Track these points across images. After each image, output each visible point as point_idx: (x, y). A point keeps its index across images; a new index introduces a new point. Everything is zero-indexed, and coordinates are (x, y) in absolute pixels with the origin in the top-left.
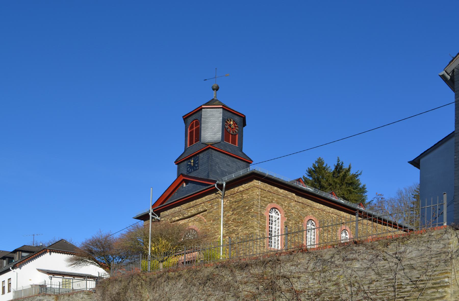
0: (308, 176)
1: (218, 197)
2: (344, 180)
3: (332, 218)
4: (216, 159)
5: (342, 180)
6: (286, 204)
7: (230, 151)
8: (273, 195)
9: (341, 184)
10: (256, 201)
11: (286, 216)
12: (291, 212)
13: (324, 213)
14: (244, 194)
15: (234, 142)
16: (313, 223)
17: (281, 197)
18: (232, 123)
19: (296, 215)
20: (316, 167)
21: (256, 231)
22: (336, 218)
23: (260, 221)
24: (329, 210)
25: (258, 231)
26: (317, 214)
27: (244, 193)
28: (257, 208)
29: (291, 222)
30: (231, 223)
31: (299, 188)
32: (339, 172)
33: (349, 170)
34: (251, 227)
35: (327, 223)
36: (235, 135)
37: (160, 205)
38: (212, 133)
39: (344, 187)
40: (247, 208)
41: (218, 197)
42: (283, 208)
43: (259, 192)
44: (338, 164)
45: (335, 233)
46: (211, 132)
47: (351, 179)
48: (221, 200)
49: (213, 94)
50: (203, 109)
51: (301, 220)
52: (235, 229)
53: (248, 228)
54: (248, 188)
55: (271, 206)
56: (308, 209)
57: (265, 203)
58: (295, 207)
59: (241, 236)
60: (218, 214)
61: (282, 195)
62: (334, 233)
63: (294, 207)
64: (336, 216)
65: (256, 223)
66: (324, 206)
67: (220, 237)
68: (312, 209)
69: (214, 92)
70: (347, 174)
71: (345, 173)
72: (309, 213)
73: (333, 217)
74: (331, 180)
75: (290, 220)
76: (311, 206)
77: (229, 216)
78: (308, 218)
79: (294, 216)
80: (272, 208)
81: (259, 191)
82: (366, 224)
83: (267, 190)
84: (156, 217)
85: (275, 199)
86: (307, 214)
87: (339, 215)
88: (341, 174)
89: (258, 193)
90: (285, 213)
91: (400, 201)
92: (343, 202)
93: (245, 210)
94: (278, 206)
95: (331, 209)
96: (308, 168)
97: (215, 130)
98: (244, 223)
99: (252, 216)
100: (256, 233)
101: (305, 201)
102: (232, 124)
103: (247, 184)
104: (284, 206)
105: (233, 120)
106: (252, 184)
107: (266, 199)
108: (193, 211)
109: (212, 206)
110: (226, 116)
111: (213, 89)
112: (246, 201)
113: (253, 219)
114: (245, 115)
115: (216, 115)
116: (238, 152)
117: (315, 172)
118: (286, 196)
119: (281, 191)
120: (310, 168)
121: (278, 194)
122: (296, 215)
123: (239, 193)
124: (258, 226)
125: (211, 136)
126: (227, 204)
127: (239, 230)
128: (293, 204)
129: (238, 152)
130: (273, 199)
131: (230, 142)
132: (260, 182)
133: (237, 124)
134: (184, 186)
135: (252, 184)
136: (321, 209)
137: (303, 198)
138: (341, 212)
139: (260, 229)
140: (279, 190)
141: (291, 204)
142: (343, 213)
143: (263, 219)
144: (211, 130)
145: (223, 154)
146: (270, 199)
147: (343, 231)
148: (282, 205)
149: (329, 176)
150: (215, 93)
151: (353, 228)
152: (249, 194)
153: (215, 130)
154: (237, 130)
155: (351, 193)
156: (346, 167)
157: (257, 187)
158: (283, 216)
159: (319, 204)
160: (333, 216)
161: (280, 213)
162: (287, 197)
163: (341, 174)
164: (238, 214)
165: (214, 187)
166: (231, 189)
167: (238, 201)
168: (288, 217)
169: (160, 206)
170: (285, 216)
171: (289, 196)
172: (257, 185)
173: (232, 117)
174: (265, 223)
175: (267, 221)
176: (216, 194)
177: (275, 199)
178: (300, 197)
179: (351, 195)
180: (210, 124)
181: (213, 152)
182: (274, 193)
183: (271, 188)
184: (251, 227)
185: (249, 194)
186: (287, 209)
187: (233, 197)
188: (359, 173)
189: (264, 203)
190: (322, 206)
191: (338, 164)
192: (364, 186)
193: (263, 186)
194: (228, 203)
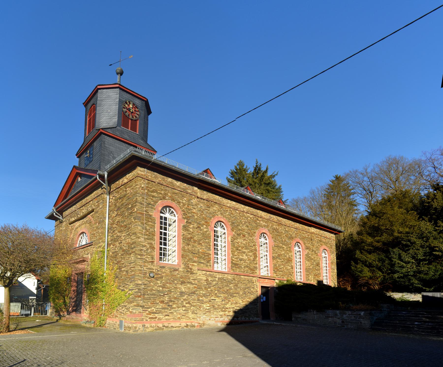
0: (231, 177)
1: (103, 193)
2: (262, 180)
3: (248, 218)
4: (111, 147)
5: (260, 180)
6: (184, 201)
7: (128, 138)
8: (166, 189)
9: (260, 184)
10: (140, 197)
11: (184, 217)
12: (192, 212)
13: (237, 212)
14: (128, 187)
15: (134, 128)
16: (222, 225)
17: (177, 191)
18: (131, 106)
19: (198, 215)
20: (237, 169)
21: (140, 240)
22: (252, 218)
23: (146, 226)
24: (243, 208)
25: (142, 239)
26: (227, 214)
27: (128, 186)
28: (142, 207)
29: (192, 226)
30: (116, 227)
31: (209, 182)
32: (258, 173)
33: (266, 171)
34: (133, 234)
35: (241, 226)
36: (137, 120)
37: (62, 202)
38: (107, 118)
39: (262, 187)
40: (130, 206)
41: (103, 193)
42: (180, 206)
43: (144, 184)
44: (256, 166)
45: (251, 238)
46: (106, 116)
47: (269, 179)
48: (107, 196)
49: (118, 79)
50: (99, 91)
51: (206, 222)
52: (119, 235)
53: (131, 234)
54: (131, 179)
55: (163, 204)
56: (216, 207)
57: (154, 199)
58: (197, 206)
59: (123, 245)
60: (103, 214)
61: (179, 189)
62: (250, 238)
63: (196, 205)
64: (252, 216)
65: (139, 228)
66: (237, 203)
67: (105, 246)
68: (222, 207)
69: (118, 76)
70: (265, 174)
71: (263, 173)
72: (218, 213)
73: (248, 217)
74: (251, 180)
75: (190, 223)
76: (219, 203)
77: (114, 217)
78: (216, 219)
79: (196, 217)
80: (166, 207)
81: (144, 182)
82: (288, 225)
83: (157, 181)
84: (60, 217)
85: (169, 194)
86: (214, 215)
87: (256, 215)
88: (260, 175)
89: (143, 186)
90: (184, 213)
91: (313, 199)
92: (260, 198)
93: (128, 209)
94: (174, 204)
95: (245, 207)
96: (231, 170)
97: (111, 113)
98: (127, 228)
99: (135, 219)
100: (140, 242)
101: (211, 197)
102: (132, 107)
103: (131, 174)
104: (182, 204)
105: (132, 103)
106: (135, 173)
107: (155, 194)
108: (84, 211)
109: (98, 204)
110: (125, 98)
111: (117, 74)
112: (129, 197)
113: (136, 222)
114: (147, 98)
115: (113, 96)
116: (139, 140)
117: (237, 173)
118: (185, 191)
119: (178, 183)
120: (233, 170)
121: (174, 188)
122: (198, 215)
123: (123, 186)
124: (143, 232)
125: (107, 120)
126: (112, 201)
127: (122, 237)
128: (194, 201)
129: (139, 140)
130: (166, 194)
131: (130, 128)
132: (146, 170)
133: (137, 108)
134: (79, 181)
135: (135, 173)
136: (233, 207)
137: (208, 193)
138: (258, 211)
139: (146, 237)
140: (175, 182)
141: (192, 201)
142: (261, 212)
143: (151, 222)
144: (107, 113)
145: (120, 142)
146: (162, 194)
147: (261, 234)
148: (179, 202)
149: (249, 177)
150: (119, 77)
151: (273, 230)
152: (132, 187)
153: (111, 113)
154: (138, 115)
155: (269, 192)
156: (263, 169)
157: (142, 176)
158: (181, 217)
159: (230, 201)
160: (249, 216)
161: (177, 214)
162: (186, 191)
163: (260, 175)
164: (122, 214)
165: (97, 181)
166: (116, 182)
167: (122, 197)
168: (187, 219)
169: (62, 203)
170: (184, 218)
171: (189, 191)
172: (142, 175)
173: (132, 100)
174: (155, 228)
175: (157, 225)
176: (102, 189)
177: (169, 194)
178: (205, 192)
179: (269, 194)
180: (105, 107)
181: (106, 138)
182: (167, 185)
183: (163, 179)
184: (133, 234)
185: (132, 187)
186: (186, 208)
187: (118, 192)
188: (275, 173)
189: (152, 199)
190: (234, 203)
191: (256, 166)
192: (280, 186)
193: (151, 176)
194: (113, 200)
